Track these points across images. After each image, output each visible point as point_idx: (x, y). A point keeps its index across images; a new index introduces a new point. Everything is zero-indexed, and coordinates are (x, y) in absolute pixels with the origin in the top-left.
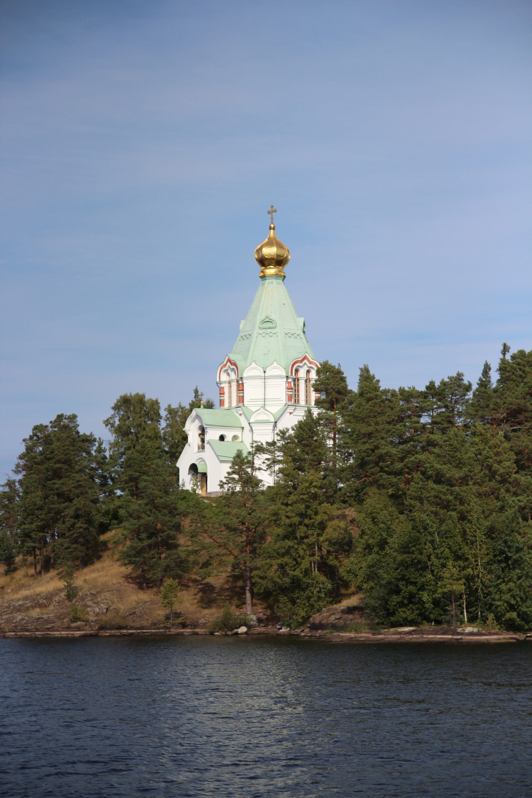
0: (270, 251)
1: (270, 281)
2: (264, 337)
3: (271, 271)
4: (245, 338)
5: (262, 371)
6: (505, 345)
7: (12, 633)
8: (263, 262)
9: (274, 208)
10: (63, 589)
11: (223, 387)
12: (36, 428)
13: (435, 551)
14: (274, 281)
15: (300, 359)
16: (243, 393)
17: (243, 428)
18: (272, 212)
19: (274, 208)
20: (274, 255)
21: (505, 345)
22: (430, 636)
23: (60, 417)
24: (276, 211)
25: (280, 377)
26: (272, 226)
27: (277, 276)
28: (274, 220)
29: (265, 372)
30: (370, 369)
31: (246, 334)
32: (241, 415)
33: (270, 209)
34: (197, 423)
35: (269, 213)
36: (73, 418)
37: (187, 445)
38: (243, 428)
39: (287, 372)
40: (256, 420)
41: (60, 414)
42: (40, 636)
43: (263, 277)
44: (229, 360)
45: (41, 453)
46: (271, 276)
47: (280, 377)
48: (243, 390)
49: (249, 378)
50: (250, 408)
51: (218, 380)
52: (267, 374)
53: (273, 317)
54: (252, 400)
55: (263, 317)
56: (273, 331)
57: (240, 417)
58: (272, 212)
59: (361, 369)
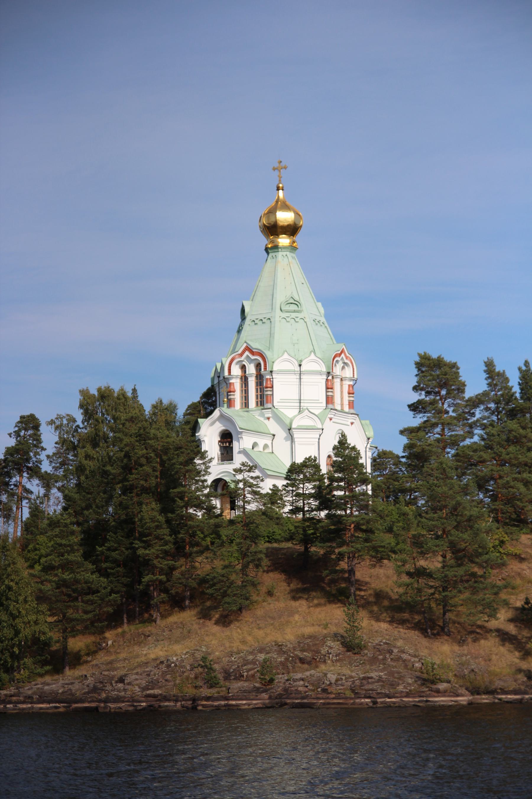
0: (284, 217)
1: (284, 253)
2: (288, 322)
3: (284, 241)
4: (260, 323)
5: (297, 364)
7: (367, 700)
8: (272, 230)
9: (283, 164)
11: (233, 383)
13: (20, 602)
14: (288, 253)
15: (339, 352)
16: (273, 391)
17: (274, 435)
18: (279, 168)
19: (283, 164)
20: (290, 220)
22: (509, 696)
24: (285, 168)
25: (320, 373)
26: (281, 185)
27: (292, 248)
28: (282, 179)
29: (300, 365)
30: (496, 363)
31: (261, 317)
32: (268, 418)
33: (277, 165)
34: (219, 427)
35: (274, 169)
38: (274, 435)
39: (327, 367)
40: (298, 426)
41: (27, 413)
42: (465, 703)
46: (285, 248)
47: (320, 373)
48: (272, 387)
49: (281, 372)
50: (281, 410)
52: (303, 368)
54: (283, 401)
56: (300, 315)
57: (266, 422)
58: (279, 168)
59: (455, 363)
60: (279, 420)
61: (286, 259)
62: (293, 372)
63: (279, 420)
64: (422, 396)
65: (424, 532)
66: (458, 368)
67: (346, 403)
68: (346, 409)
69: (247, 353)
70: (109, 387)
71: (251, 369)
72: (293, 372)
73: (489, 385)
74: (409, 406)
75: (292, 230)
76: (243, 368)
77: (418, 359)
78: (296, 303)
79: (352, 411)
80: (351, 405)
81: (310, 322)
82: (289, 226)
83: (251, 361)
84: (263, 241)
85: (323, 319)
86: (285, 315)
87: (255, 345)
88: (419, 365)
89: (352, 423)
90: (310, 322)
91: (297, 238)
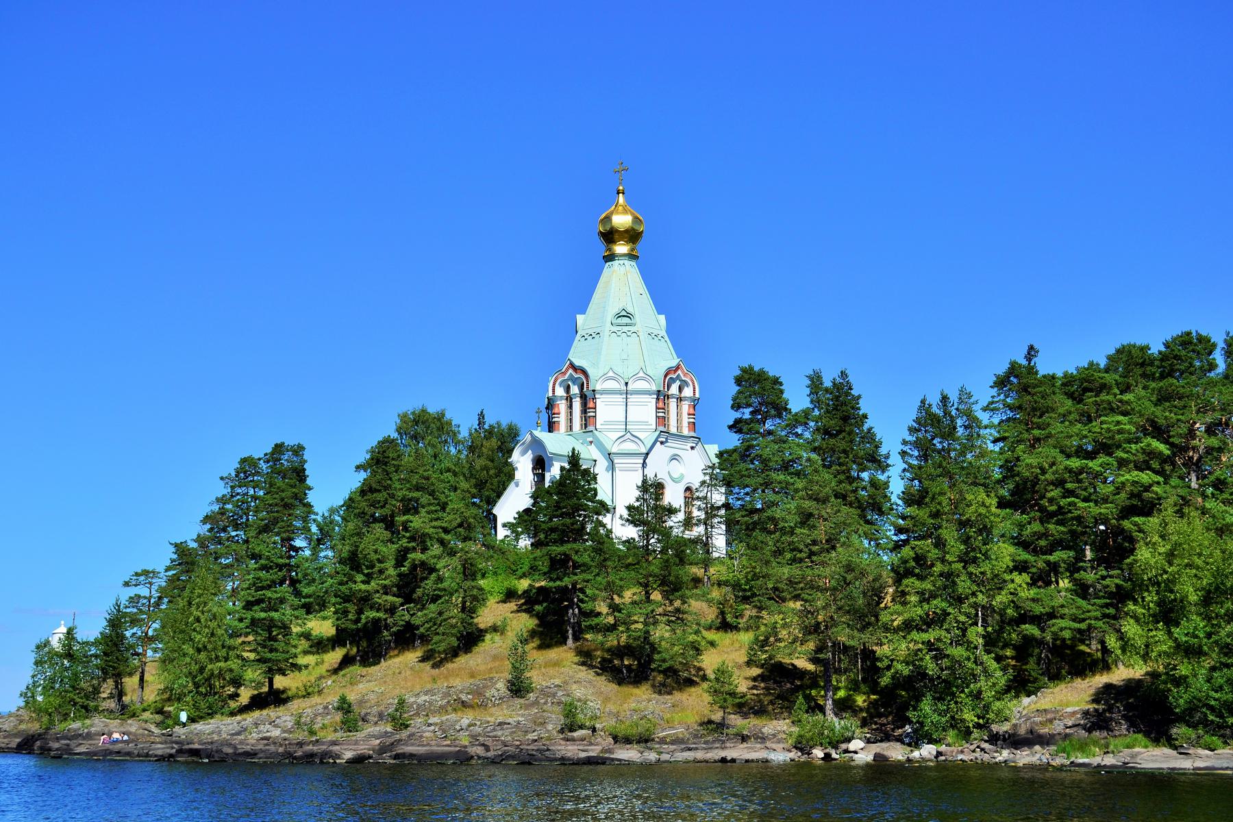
0: (622, 220)
6: (1031, 348)
8: (610, 236)
10: (1186, 717)
12: (243, 461)
14: (626, 262)
21: (1031, 348)
23: (279, 448)
25: (648, 393)
27: (632, 256)
36: (298, 450)
37: (512, 485)
43: (610, 257)
44: (572, 366)
45: (448, 452)
47: (648, 393)
49: (604, 392)
51: (550, 394)
52: (630, 387)
53: (630, 310)
54: (606, 423)
55: (616, 311)
56: (632, 329)
60: (601, 447)
61: (622, 268)
62: (619, 392)
63: (601, 447)
64: (746, 414)
65: (381, 615)
66: (781, 384)
67: (685, 424)
68: (686, 432)
69: (571, 371)
70: (443, 415)
71: (575, 390)
72: (619, 392)
73: (812, 402)
74: (730, 427)
75: (632, 236)
76: (568, 389)
77: (738, 372)
78: (629, 316)
79: (692, 434)
80: (693, 426)
81: (643, 335)
82: (627, 231)
83: (574, 381)
84: (600, 245)
85: (664, 333)
86: (615, 329)
87: (577, 363)
88: (738, 381)
89: (692, 448)
90: (643, 335)
91: (638, 245)
